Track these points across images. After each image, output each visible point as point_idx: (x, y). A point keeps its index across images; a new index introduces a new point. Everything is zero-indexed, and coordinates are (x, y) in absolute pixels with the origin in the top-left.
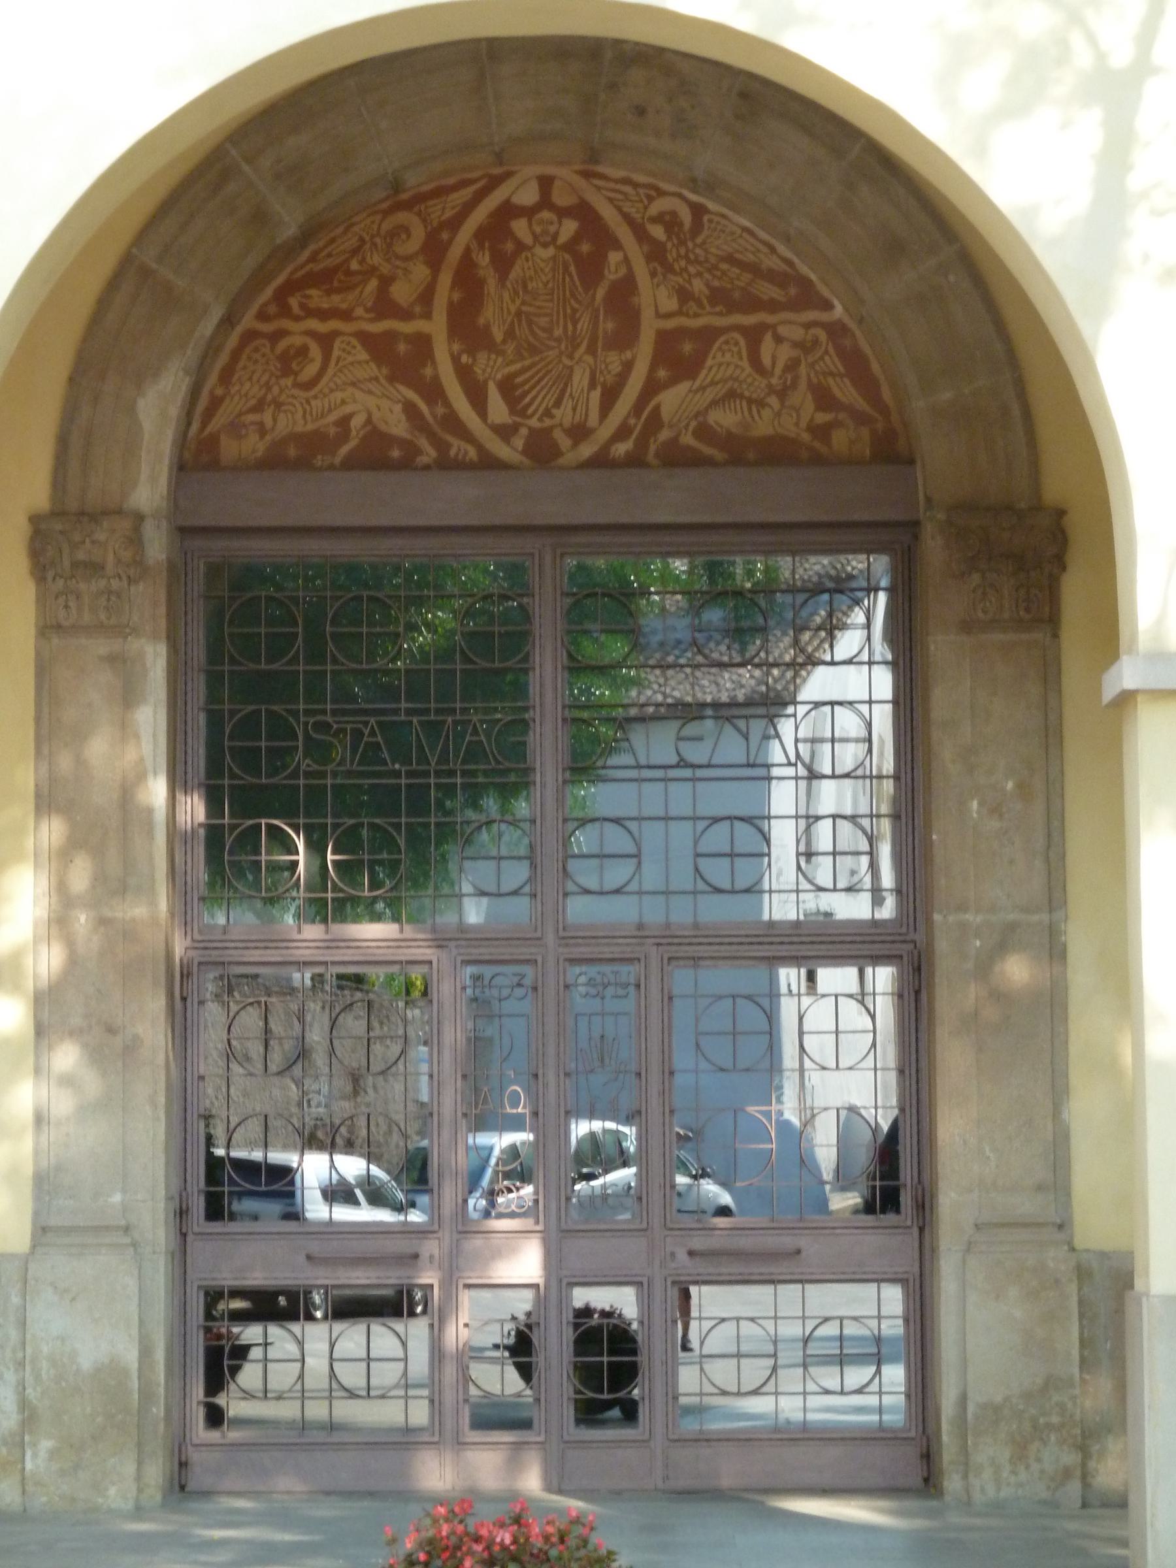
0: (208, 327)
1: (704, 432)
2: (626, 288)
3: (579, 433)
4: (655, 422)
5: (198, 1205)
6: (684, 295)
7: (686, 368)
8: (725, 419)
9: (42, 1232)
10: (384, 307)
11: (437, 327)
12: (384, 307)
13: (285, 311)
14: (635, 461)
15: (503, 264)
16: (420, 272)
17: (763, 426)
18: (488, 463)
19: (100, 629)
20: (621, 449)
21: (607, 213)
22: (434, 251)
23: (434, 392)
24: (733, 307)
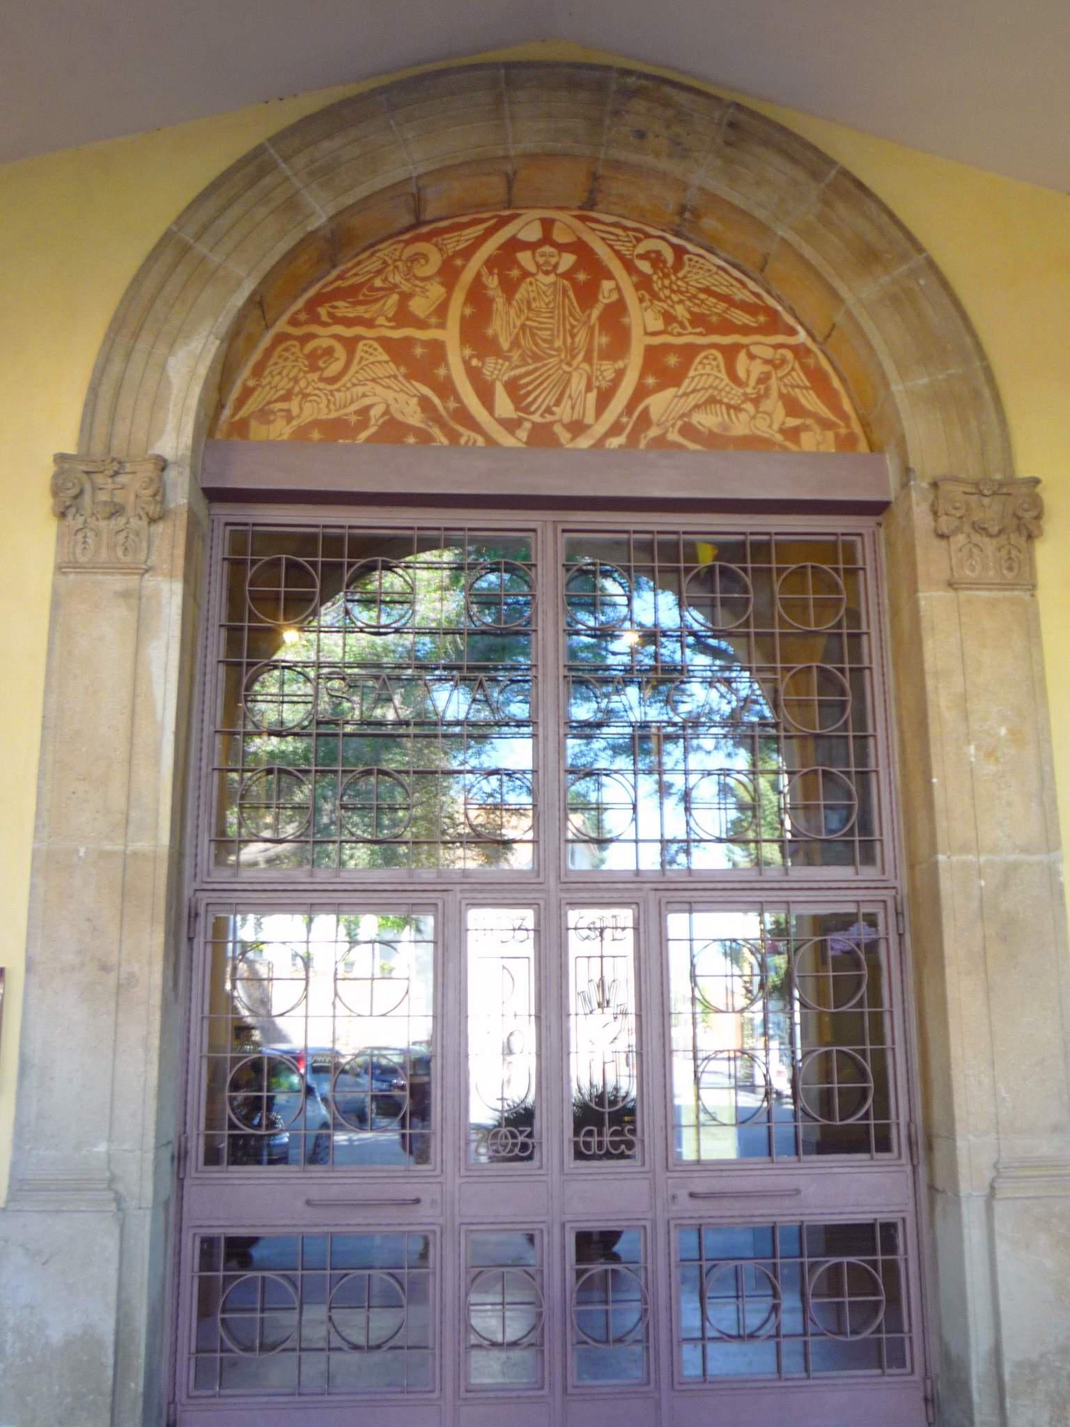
1: (688, 430)
2: (618, 308)
3: (577, 428)
5: (197, 1148)
6: (669, 318)
7: (672, 378)
8: (707, 420)
10: (403, 317)
11: (450, 336)
12: (403, 317)
15: (509, 288)
16: (436, 290)
17: (740, 426)
22: (449, 274)
23: (446, 389)
24: (711, 329)
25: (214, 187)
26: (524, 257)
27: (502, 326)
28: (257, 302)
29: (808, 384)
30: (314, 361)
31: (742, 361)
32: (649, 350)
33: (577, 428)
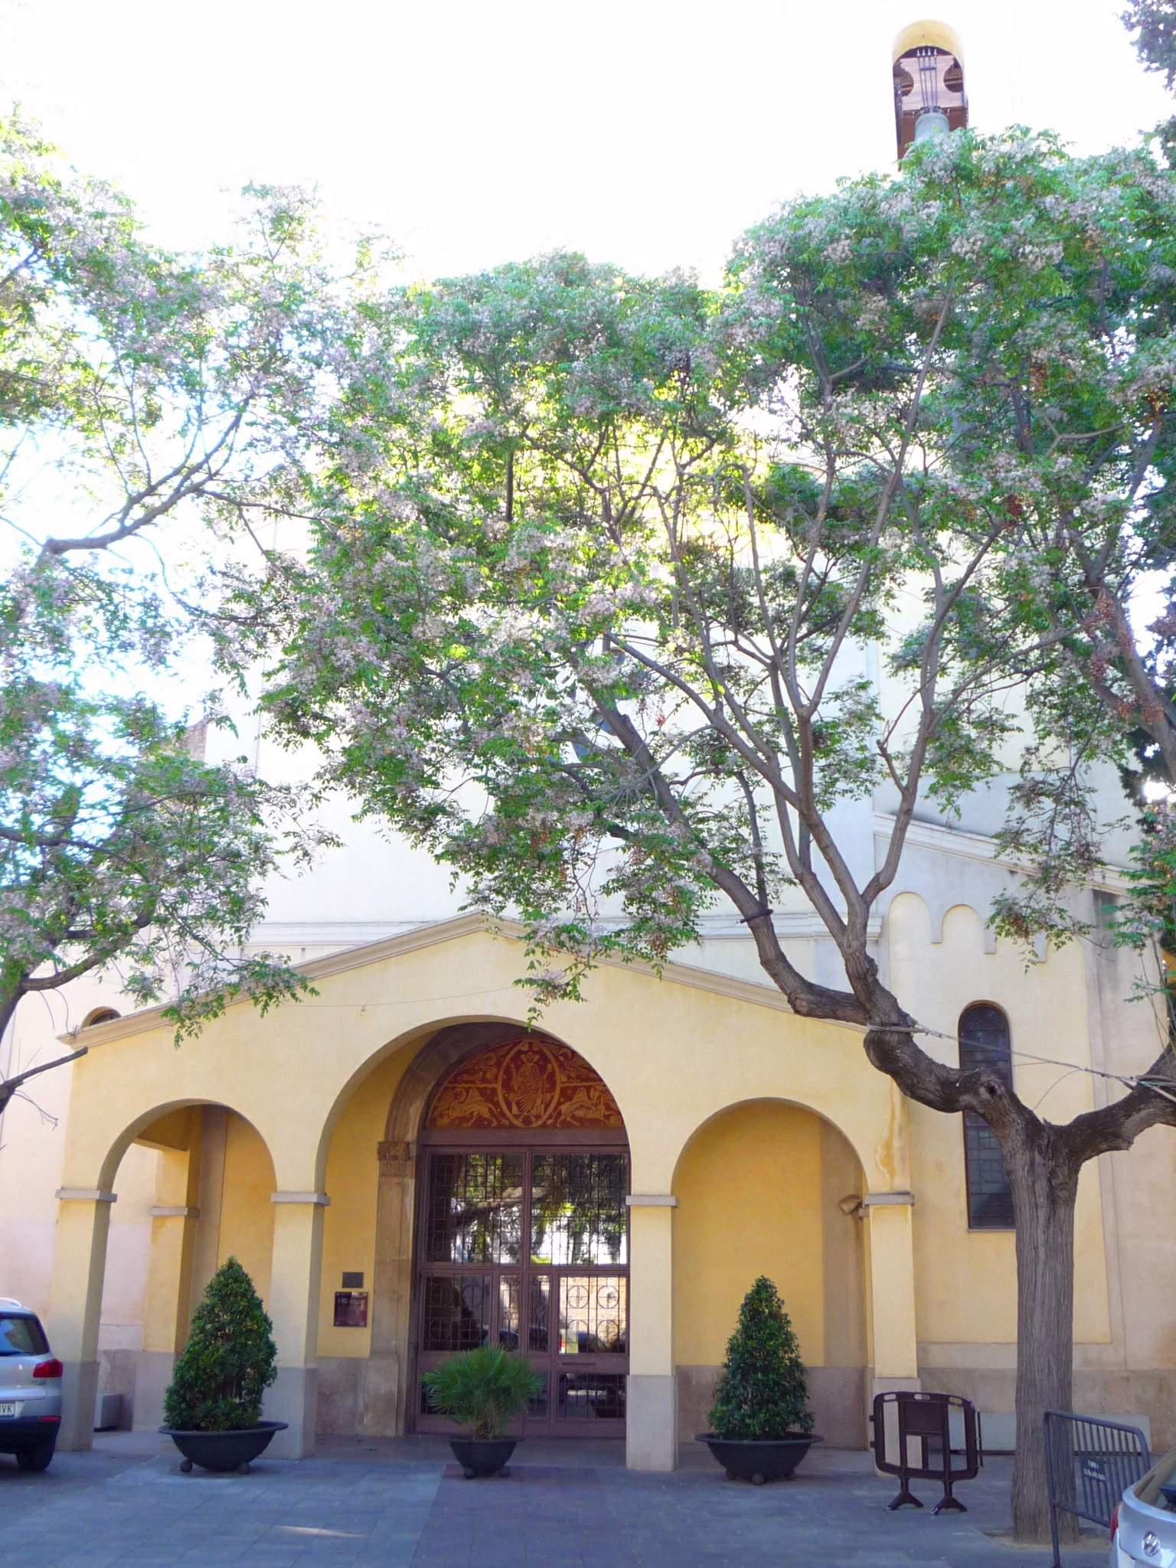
0: (430, 1088)
1: (573, 1117)
2: (552, 1075)
3: (538, 1117)
4: (560, 1114)
5: (421, 1346)
6: (569, 1077)
7: (569, 1098)
8: (580, 1113)
9: (374, 1352)
10: (484, 1080)
11: (498, 1086)
12: (484, 1080)
13: (456, 1081)
14: (554, 1125)
15: (518, 1068)
16: (495, 1070)
17: (591, 1115)
18: (513, 1126)
19: (395, 1175)
20: (550, 1122)
21: (548, 1053)
22: (499, 1064)
23: (497, 1105)
24: (582, 1080)
25: (421, 1053)
26: (523, 1057)
27: (515, 1083)
28: (438, 1085)
29: (1120, 675)
30: (457, 1096)
31: (592, 1092)
32: (562, 1089)
33: (538, 1117)
